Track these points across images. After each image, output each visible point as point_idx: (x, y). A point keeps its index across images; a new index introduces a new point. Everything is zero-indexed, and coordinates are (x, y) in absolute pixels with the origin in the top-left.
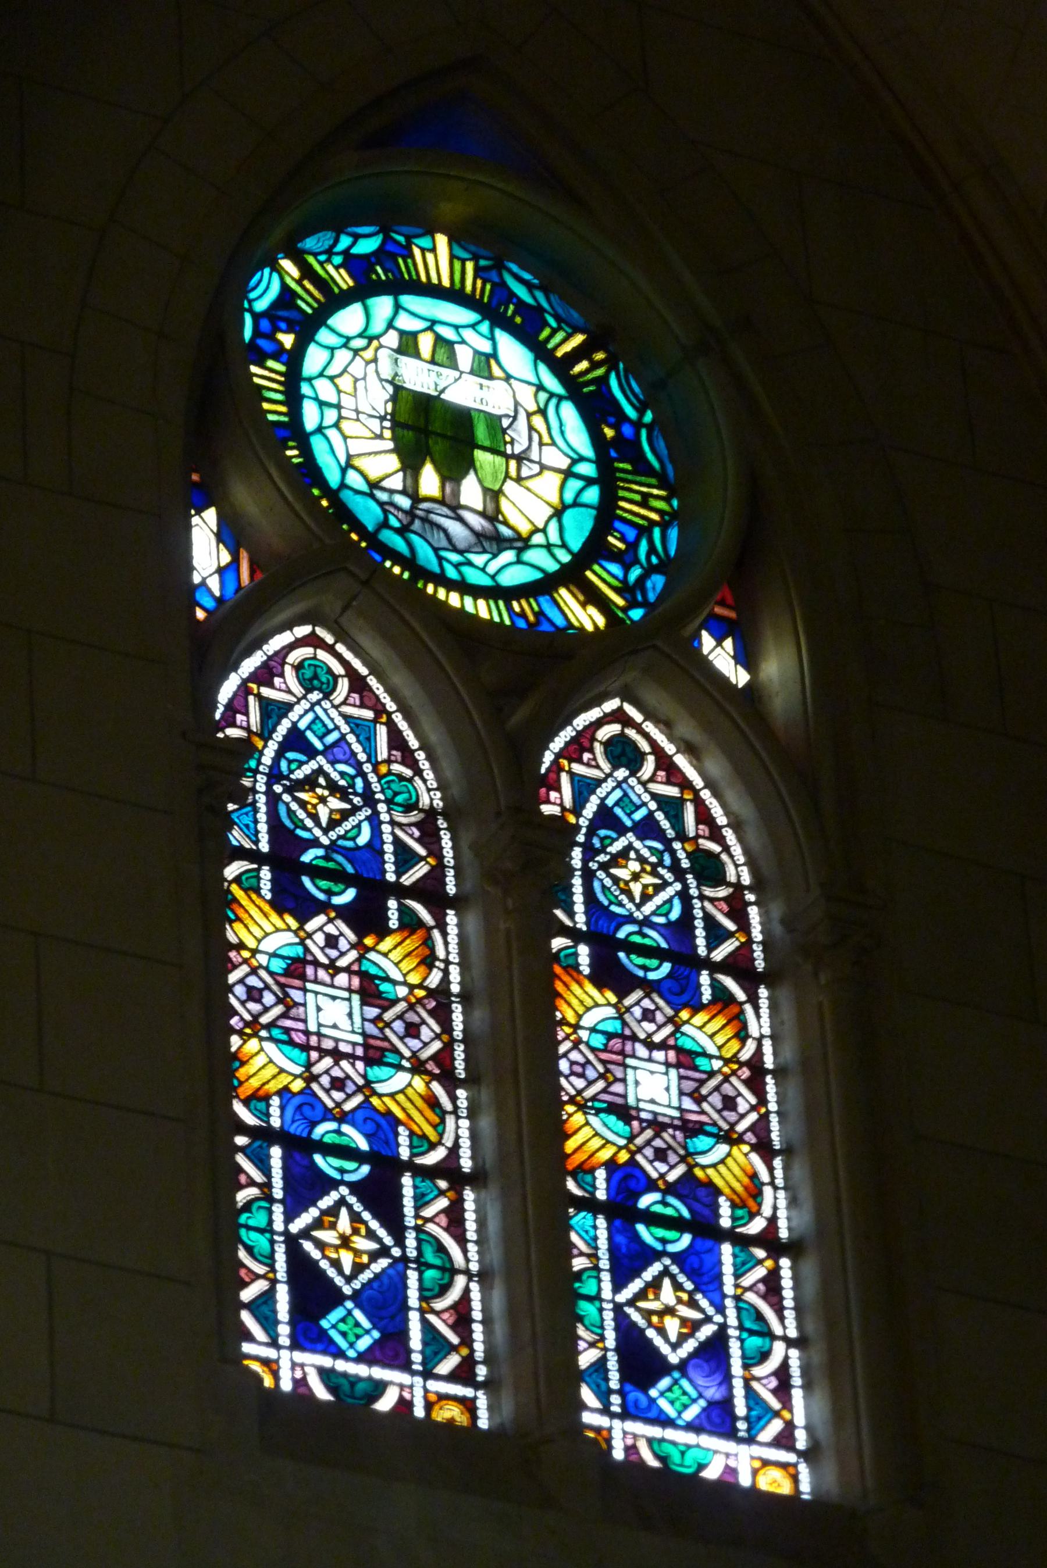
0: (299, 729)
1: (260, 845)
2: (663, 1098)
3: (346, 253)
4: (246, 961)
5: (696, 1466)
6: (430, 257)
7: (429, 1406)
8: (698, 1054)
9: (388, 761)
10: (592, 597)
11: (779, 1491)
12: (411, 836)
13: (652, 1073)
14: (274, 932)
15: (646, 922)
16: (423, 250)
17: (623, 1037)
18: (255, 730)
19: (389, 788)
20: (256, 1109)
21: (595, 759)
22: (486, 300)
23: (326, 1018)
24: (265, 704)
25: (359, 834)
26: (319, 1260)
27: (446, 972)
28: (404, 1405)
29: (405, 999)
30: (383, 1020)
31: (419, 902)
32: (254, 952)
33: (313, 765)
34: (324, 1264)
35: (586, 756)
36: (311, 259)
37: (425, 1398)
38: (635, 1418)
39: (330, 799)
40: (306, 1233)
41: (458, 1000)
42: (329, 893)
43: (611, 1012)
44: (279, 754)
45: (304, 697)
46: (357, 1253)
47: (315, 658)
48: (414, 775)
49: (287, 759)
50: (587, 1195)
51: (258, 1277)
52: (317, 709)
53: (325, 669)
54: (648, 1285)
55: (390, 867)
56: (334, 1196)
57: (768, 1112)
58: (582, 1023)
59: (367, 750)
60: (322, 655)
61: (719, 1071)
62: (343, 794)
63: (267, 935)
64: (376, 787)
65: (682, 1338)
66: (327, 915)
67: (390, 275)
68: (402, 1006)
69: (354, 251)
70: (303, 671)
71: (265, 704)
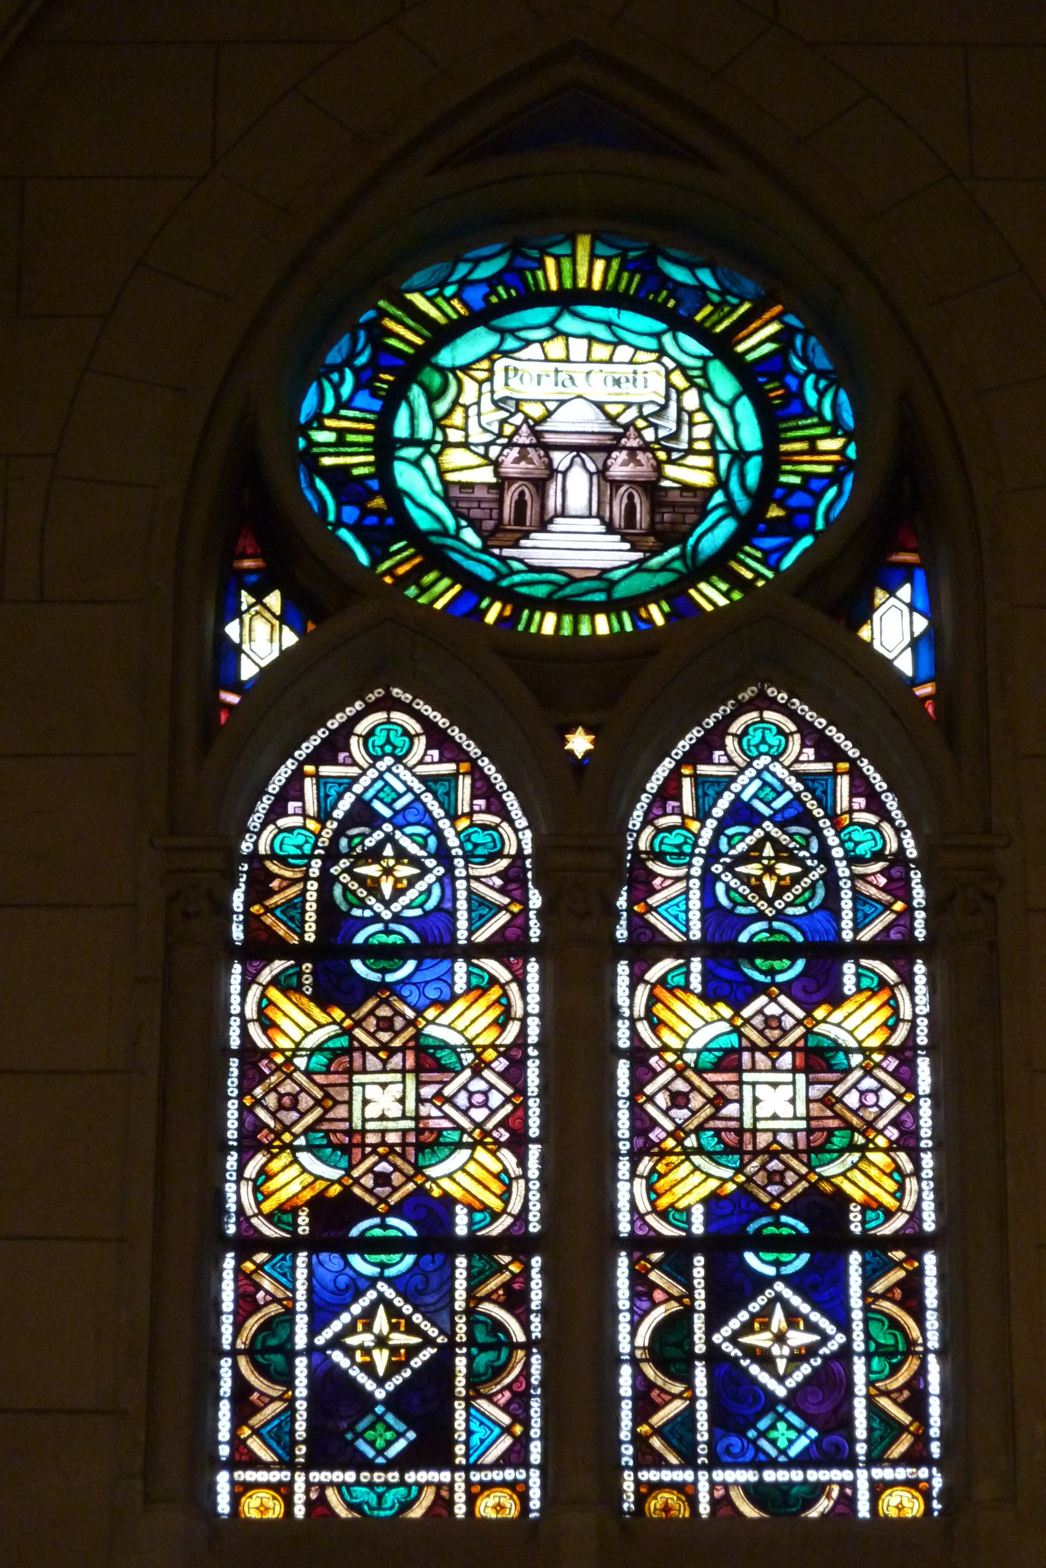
4: (279, 1068)
6: (566, 265)
7: (471, 1501)
9: (851, 811)
11: (270, 1515)
14: (704, 1026)
15: (397, 918)
17: (348, 1051)
19: (469, 840)
21: (351, 756)
22: (632, 292)
23: (395, 1111)
25: (811, 899)
27: (524, 1027)
28: (443, 1502)
31: (874, 958)
32: (679, 1053)
33: (759, 833)
34: (355, 1372)
38: (724, 1466)
40: (336, 1342)
41: (924, 1053)
42: (772, 972)
43: (725, 1027)
44: (718, 832)
48: (653, 825)
53: (774, 730)
55: (462, 924)
56: (769, 1293)
57: (240, 1097)
58: (688, 1046)
59: (446, 806)
60: (397, 716)
63: (695, 1031)
64: (453, 841)
68: (858, 1074)
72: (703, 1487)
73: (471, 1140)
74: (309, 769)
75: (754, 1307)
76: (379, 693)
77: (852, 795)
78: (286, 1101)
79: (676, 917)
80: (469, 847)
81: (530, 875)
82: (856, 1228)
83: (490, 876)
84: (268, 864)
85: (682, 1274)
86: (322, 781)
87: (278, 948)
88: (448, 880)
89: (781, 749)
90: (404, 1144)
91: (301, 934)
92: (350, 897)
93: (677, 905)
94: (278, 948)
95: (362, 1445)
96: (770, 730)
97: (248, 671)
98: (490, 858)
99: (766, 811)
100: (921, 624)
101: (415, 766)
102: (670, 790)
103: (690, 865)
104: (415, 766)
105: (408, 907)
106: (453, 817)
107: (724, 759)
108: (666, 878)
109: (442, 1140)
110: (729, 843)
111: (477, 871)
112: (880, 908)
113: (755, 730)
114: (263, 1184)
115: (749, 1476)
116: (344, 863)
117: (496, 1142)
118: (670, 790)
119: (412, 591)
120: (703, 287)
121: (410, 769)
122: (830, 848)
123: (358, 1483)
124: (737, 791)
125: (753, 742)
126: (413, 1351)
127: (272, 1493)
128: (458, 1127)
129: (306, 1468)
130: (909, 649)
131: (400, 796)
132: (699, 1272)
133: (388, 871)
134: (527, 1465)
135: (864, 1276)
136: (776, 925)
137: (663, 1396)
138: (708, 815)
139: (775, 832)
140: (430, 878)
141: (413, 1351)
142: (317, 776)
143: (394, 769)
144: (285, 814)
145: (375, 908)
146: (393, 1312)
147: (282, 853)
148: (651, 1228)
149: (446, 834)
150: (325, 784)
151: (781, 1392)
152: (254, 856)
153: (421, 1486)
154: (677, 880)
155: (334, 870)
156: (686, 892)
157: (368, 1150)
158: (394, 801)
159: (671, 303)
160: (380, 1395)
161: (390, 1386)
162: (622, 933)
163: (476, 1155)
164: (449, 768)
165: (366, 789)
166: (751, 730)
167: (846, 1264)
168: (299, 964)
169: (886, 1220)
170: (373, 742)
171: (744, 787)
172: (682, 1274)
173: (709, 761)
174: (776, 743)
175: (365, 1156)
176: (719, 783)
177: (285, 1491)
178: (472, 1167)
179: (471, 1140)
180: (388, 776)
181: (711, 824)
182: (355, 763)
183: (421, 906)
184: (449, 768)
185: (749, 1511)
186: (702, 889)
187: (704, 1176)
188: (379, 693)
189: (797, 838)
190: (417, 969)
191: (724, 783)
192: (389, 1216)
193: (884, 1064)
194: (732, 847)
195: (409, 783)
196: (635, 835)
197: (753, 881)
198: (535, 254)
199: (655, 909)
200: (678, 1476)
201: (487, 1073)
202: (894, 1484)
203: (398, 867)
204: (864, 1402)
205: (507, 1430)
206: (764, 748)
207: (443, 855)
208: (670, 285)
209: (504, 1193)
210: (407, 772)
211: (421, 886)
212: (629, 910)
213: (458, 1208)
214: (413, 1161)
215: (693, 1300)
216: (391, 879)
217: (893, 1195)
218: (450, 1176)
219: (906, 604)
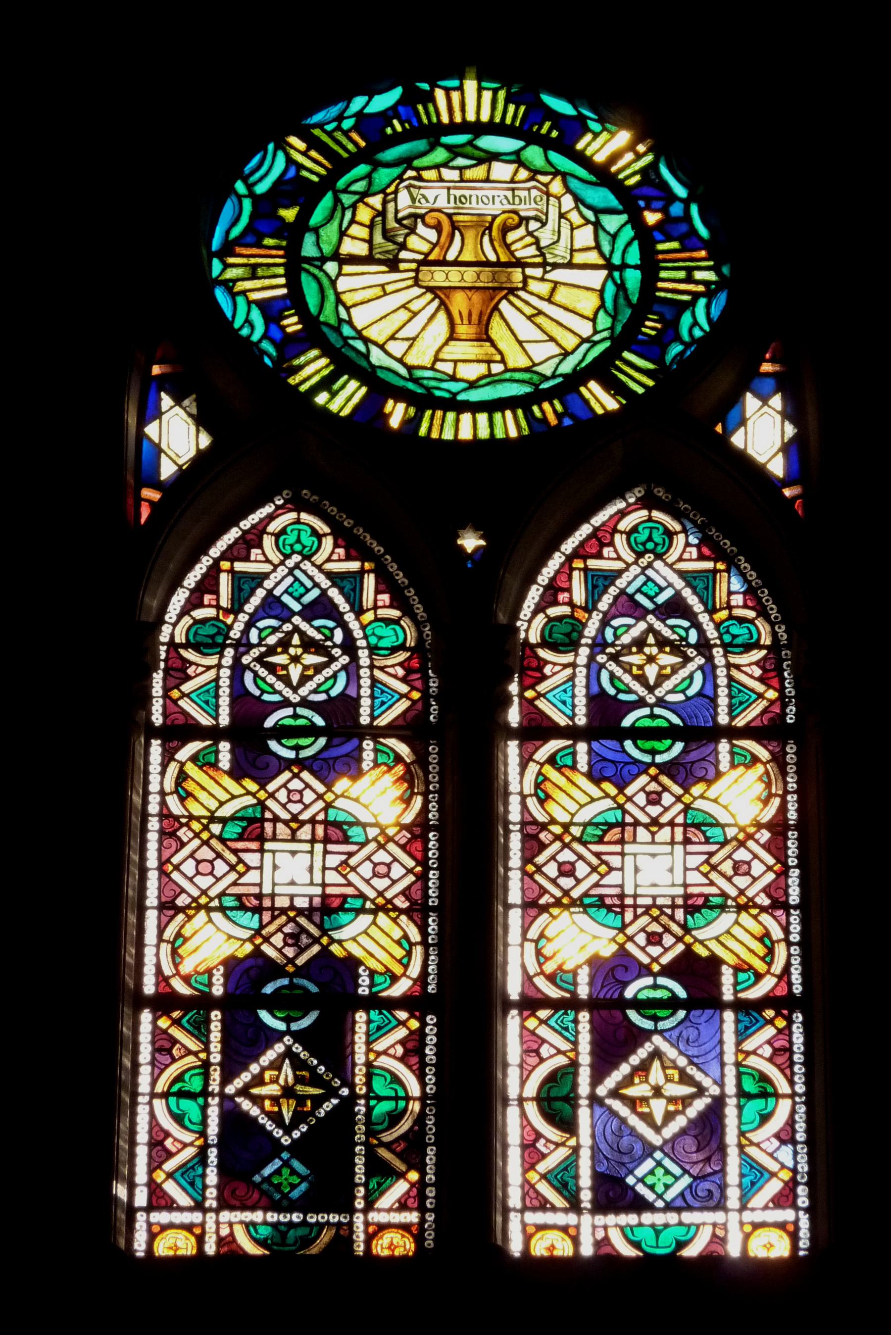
0: (275, 596)
1: (576, 720)
2: (641, 879)
3: (359, 115)
4: (558, 838)
5: (674, 1245)
8: (351, 824)
10: (614, 386)
12: (395, 676)
13: (654, 855)
15: (305, 703)
16: (447, 90)
17: (622, 825)
18: (579, 604)
19: (728, 632)
20: (562, 980)
24: (237, 578)
26: (688, 1118)
28: (718, 1240)
29: (375, 839)
30: (348, 865)
32: (566, 827)
35: (607, 551)
36: (317, 132)
37: (524, 1230)
39: (661, 656)
40: (244, 1092)
44: (249, 625)
45: (282, 563)
46: (301, 1100)
47: (650, 519)
50: (568, 995)
52: (650, 572)
53: (661, 529)
54: (635, 1070)
61: (735, 838)
62: (676, 648)
65: (669, 1117)
66: (291, 771)
67: (407, 125)
69: (367, 110)
70: (636, 535)
71: (237, 578)
72: (210, 1226)
73: (373, 907)
74: (225, 565)
75: (635, 1060)
77: (377, 592)
80: (727, 638)
81: (162, 665)
83: (393, 666)
84: (182, 652)
85: (200, 1030)
86: (590, 574)
87: (192, 731)
88: (709, 670)
89: (314, 548)
90: (674, 907)
91: (216, 718)
92: (260, 682)
94: (192, 731)
95: (641, 1189)
96: (658, 529)
97: (167, 470)
98: (394, 650)
99: (296, 607)
100: (790, 430)
102: (209, 583)
103: (222, 656)
105: (672, 691)
106: (359, 611)
107: (614, 555)
109: (347, 906)
110: (615, 634)
111: (734, 659)
112: (754, 696)
114: (180, 946)
116: (255, 652)
117: (395, 909)
118: (209, 583)
119: (321, 398)
121: (670, 566)
122: (355, 640)
123: (640, 1225)
124: (269, 588)
125: (287, 542)
126: (686, 1101)
127: (401, 1232)
128: (362, 896)
130: (781, 454)
131: (308, 590)
132: (216, 1028)
133: (296, 659)
134: (726, 1210)
135: (737, 1033)
136: (657, 711)
137: (549, 1145)
138: (241, 610)
139: (304, 626)
141: (686, 1101)
142: (231, 571)
143: (302, 565)
144: (201, 605)
145: (284, 693)
147: (550, 640)
148: (538, 990)
149: (351, 626)
150: (240, 579)
152: (172, 645)
154: (565, 666)
155: (246, 660)
156: (572, 678)
157: (640, 911)
158: (302, 596)
159: (555, 134)
161: (296, 1134)
162: (514, 716)
164: (355, 566)
165: (629, 583)
168: (216, 744)
169: (756, 982)
170: (285, 539)
171: (629, 583)
172: (200, 1030)
173: (247, 559)
174: (310, 544)
175: (636, 917)
178: (373, 931)
179: (373, 907)
180: (297, 573)
181: (243, 618)
182: (619, 558)
184: (355, 566)
186: (231, 678)
190: (684, 751)
191: (612, 577)
192: (296, 977)
193: (757, 836)
194: (617, 637)
195: (317, 580)
197: (635, 670)
198: (425, 86)
199: (544, 695)
200: (561, 1219)
201: (751, 844)
202: (171, 1226)
203: (305, 656)
206: (650, 546)
207: (704, 646)
208: (390, 113)
209: (766, 955)
210: (667, 569)
211: (683, 673)
212: (521, 696)
213: (724, 968)
215: (577, 1054)
216: (300, 667)
217: (762, 959)
218: (354, 939)
219: (778, 412)
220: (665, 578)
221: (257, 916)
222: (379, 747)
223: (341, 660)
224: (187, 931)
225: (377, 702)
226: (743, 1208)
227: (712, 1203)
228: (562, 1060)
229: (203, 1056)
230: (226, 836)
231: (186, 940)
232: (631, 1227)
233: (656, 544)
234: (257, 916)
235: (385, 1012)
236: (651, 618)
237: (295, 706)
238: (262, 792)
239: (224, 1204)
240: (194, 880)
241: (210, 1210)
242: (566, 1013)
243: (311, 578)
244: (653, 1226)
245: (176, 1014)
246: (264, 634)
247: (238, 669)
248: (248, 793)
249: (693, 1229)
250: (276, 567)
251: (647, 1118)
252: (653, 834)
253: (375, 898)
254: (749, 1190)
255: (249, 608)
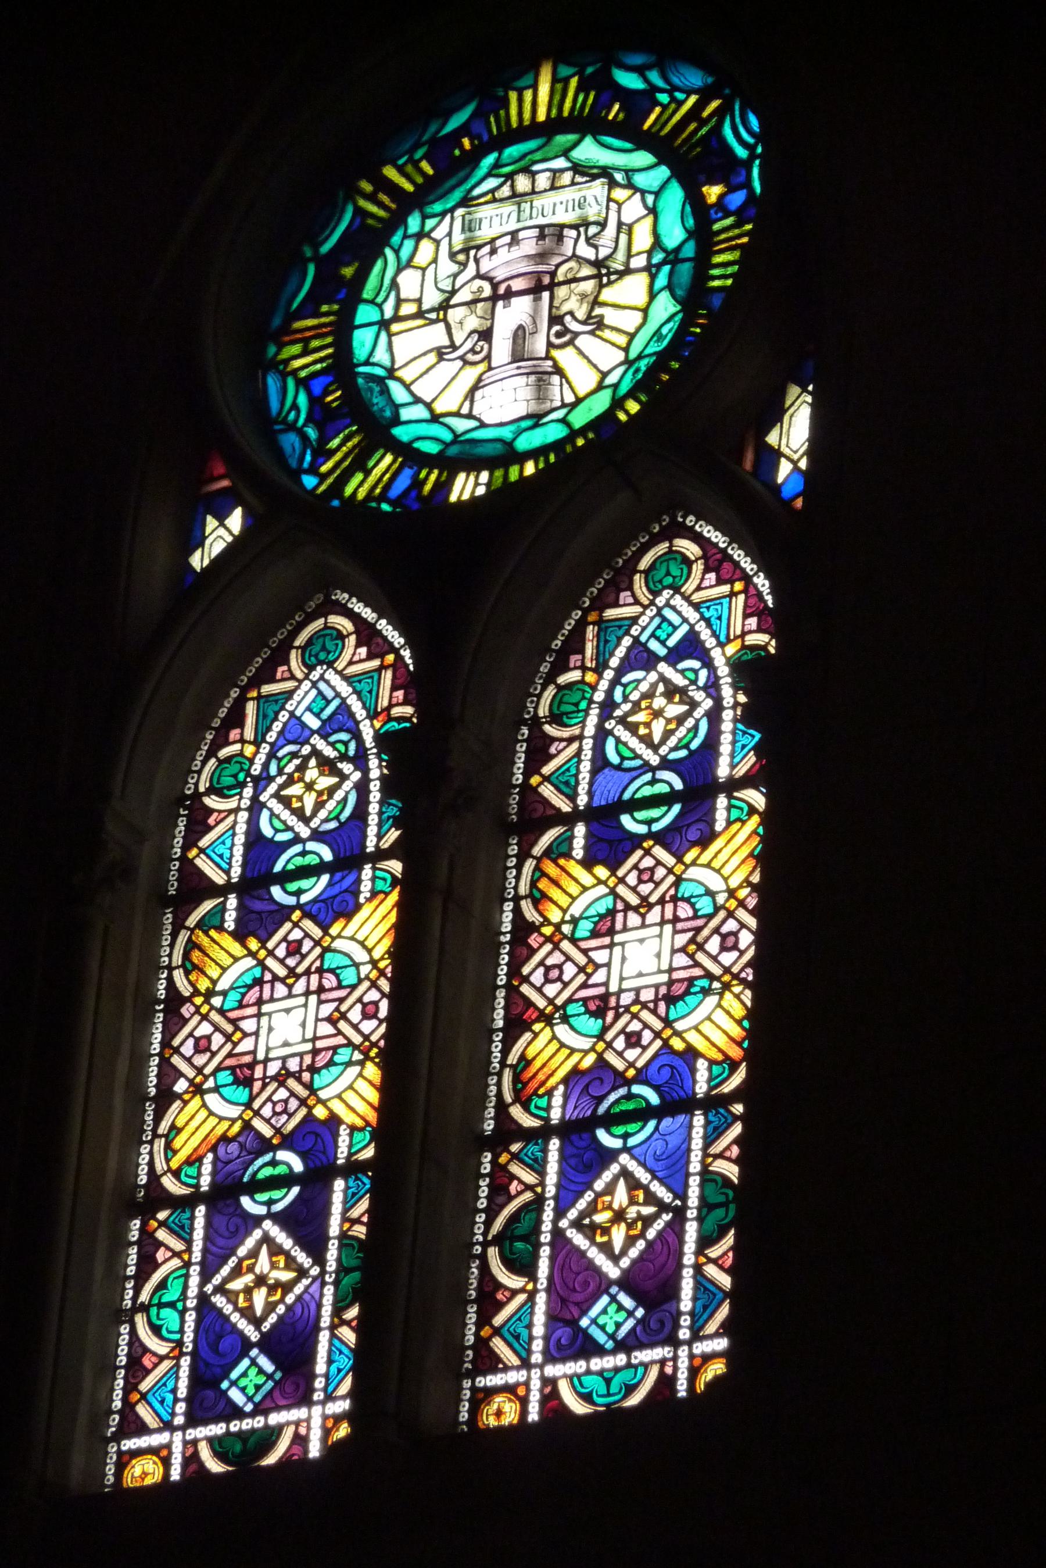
4: (548, 939)
14: (233, 963)
15: (666, 764)
21: (290, 670)
23: (295, 1036)
29: (367, 978)
32: (558, 927)
40: (220, 1289)
49: (349, 741)
51: (714, 1261)
72: (177, 1448)
76: (320, 598)
78: (731, 940)
79: (221, 856)
82: (701, 1089)
90: (656, 1001)
93: (223, 843)
99: (662, 652)
101: (344, 669)
104: (344, 669)
105: (675, 749)
108: (220, 812)
113: (661, 563)
115: (218, 1429)
116: (272, 788)
120: (654, 89)
123: (588, 1372)
126: (648, 1221)
129: (183, 1428)
140: (348, 785)
146: (634, 1184)
151: (613, 1272)
153: (646, 1366)
154: (570, 740)
157: (621, 1010)
160: (613, 1272)
163: (365, 1073)
166: (658, 565)
167: (330, 1191)
176: (276, 701)
177: (163, 1454)
183: (337, 818)
185: (215, 1466)
187: (217, 1120)
188: (320, 598)
189: (688, 674)
195: (338, 689)
196: (196, 775)
204: (691, 1271)
205: (497, 1332)
214: (663, 1015)
218: (696, 1028)
220: (333, 688)
221: (247, 1090)
222: (734, 802)
223: (268, 797)
224: (531, 1053)
225: (739, 745)
226: (696, 1336)
227: (662, 1336)
228: (528, 1196)
229: (186, 1257)
230: (578, 935)
231: (179, 1131)
232: (579, 1376)
233: (674, 577)
234: (247, 1090)
235: (360, 1175)
236: (662, 667)
237: (653, 769)
238: (613, 879)
239: (550, 1357)
240: (719, 958)
241: (536, 1366)
242: (183, 1211)
243: (679, 613)
244: (600, 1373)
245: (515, 1148)
246: (283, 763)
247: (256, 807)
248: (600, 882)
249: (641, 1370)
250: (300, 682)
251: (606, 1248)
252: (643, 916)
253: (722, 976)
254: (702, 1315)
255: (614, 662)
